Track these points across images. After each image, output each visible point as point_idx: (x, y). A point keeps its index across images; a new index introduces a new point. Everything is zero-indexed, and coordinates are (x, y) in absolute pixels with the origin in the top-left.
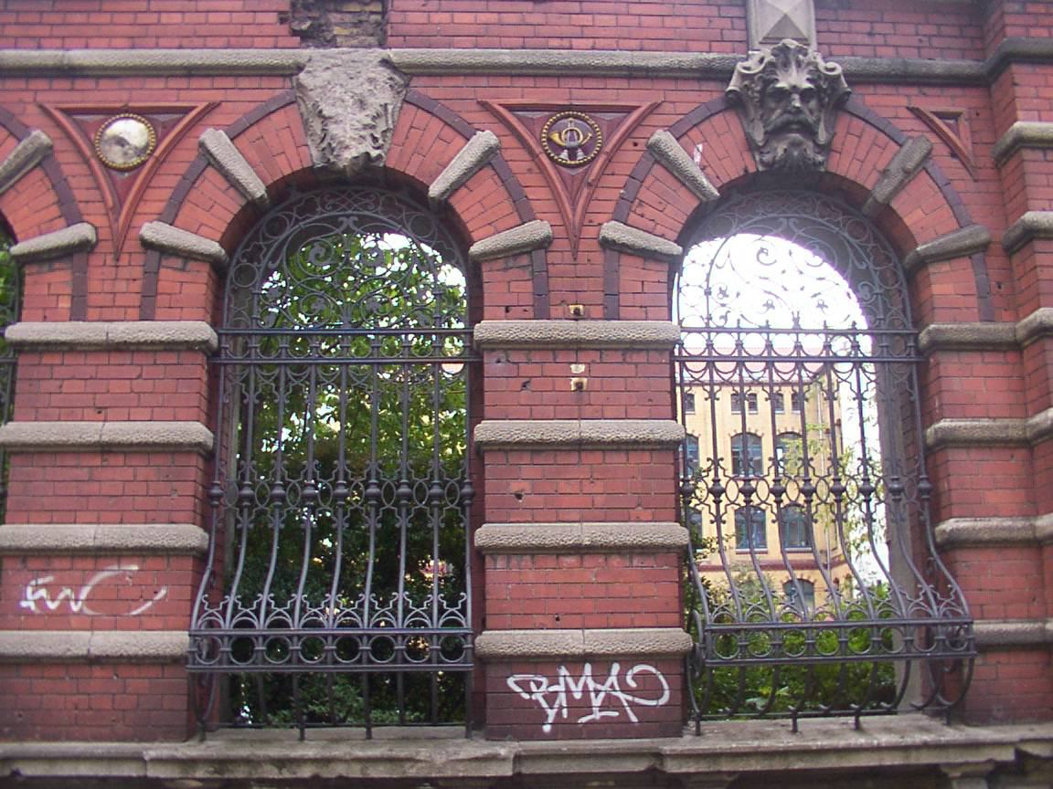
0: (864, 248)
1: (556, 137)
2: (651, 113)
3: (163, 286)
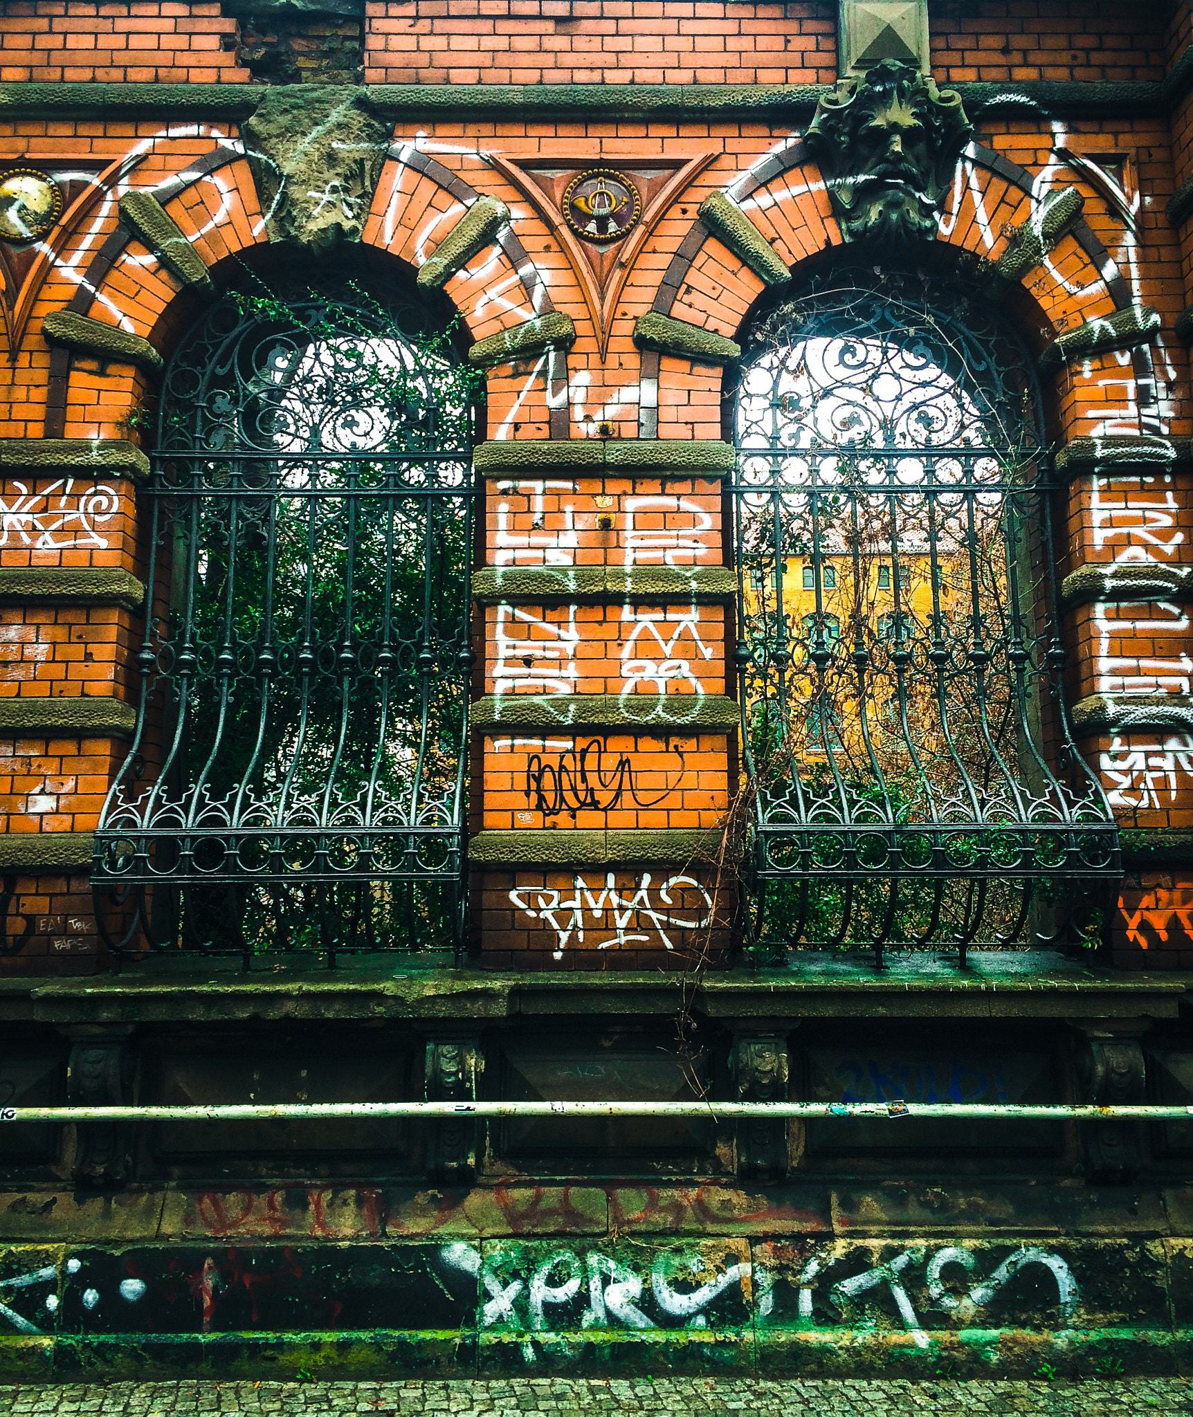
0: (985, 343)
1: (581, 203)
2: (705, 169)
3: (74, 395)
